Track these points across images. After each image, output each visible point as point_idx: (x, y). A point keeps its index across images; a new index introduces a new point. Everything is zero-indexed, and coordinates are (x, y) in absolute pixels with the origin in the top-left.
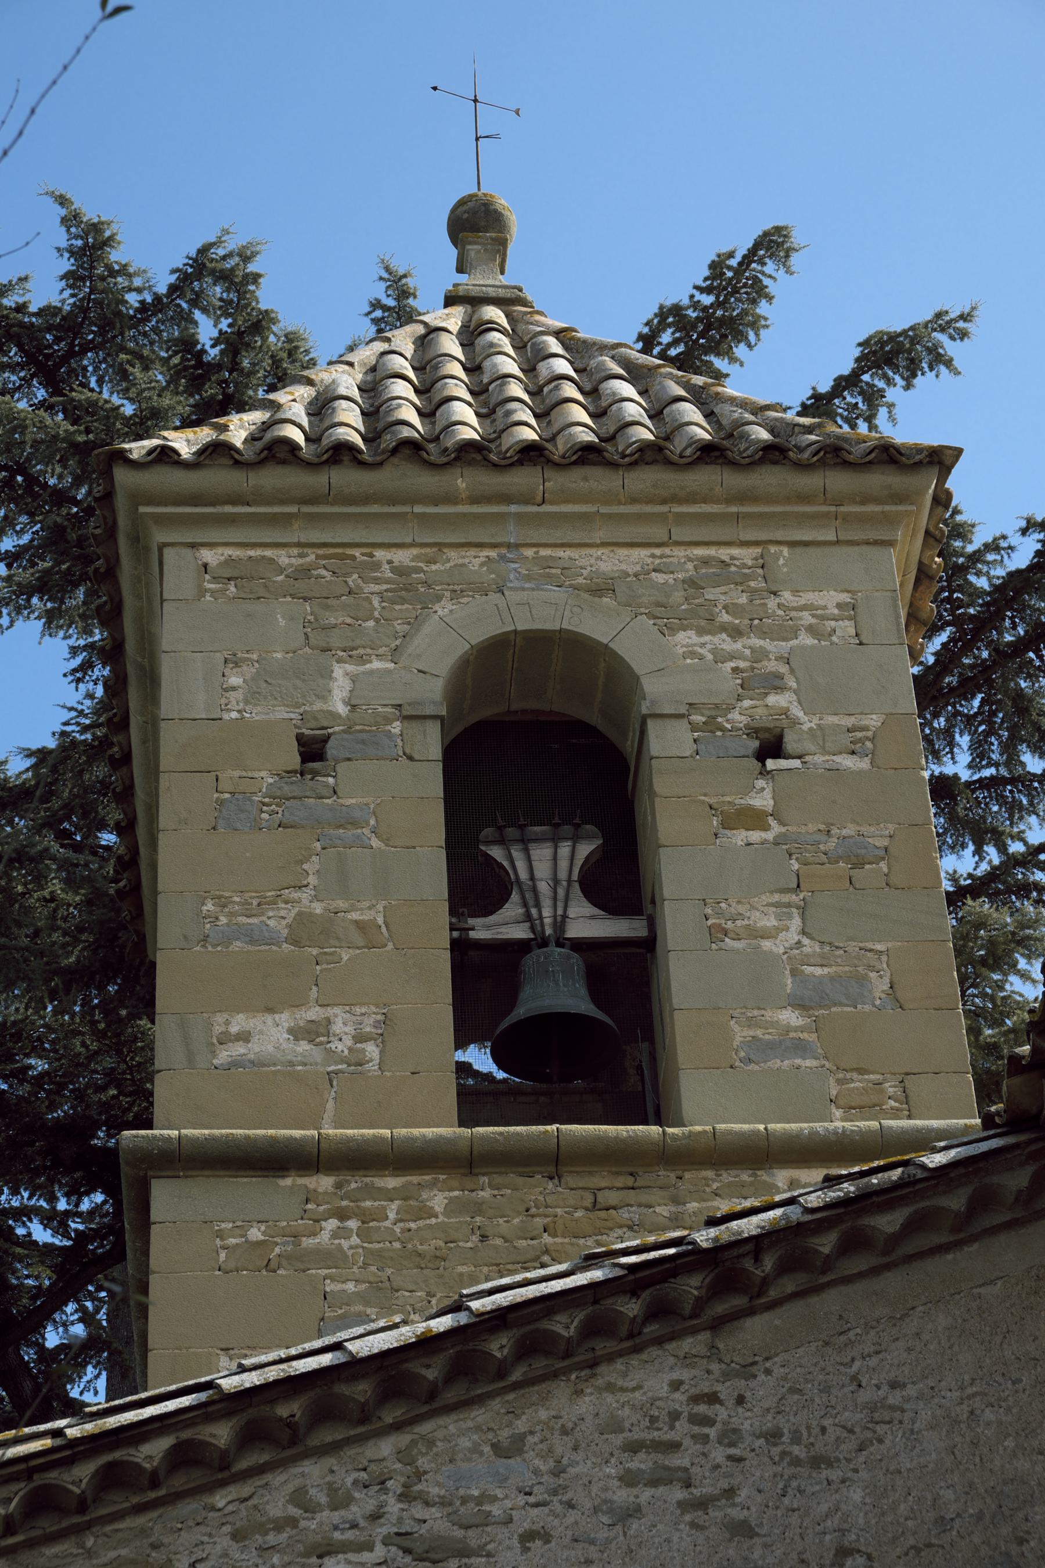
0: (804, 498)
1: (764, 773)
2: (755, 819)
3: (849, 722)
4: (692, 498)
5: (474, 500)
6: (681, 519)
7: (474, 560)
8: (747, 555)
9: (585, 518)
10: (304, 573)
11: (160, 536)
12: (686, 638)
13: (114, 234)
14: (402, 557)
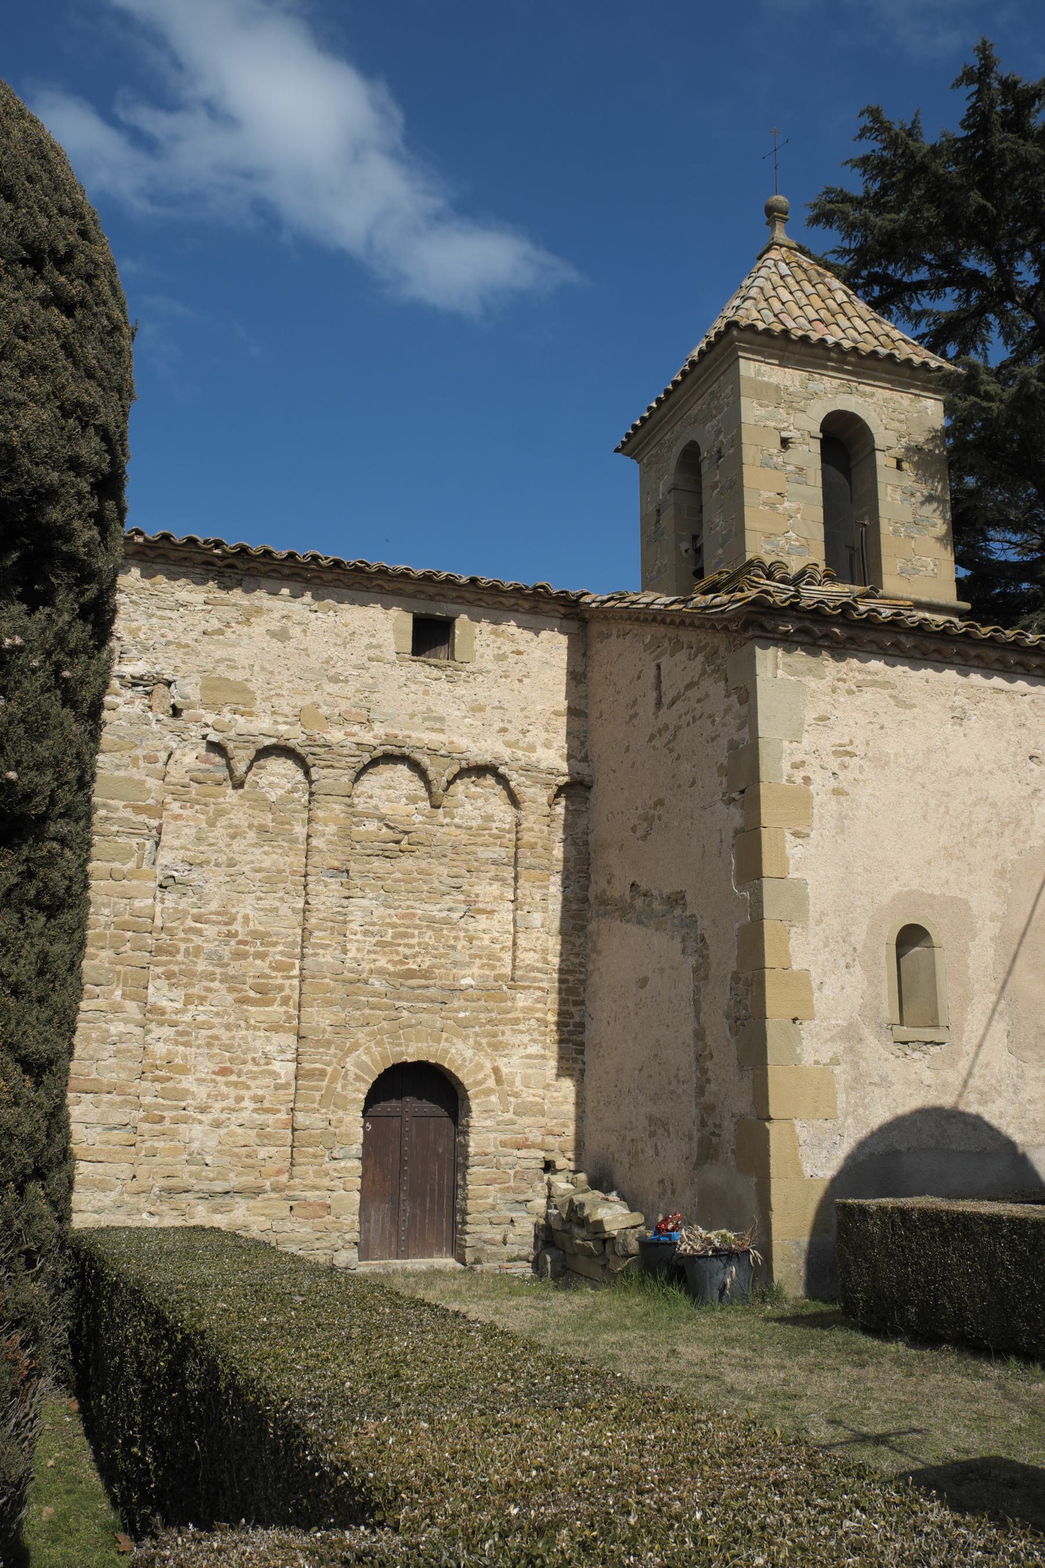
4: (699, 379)
7: (677, 428)
11: (740, 354)
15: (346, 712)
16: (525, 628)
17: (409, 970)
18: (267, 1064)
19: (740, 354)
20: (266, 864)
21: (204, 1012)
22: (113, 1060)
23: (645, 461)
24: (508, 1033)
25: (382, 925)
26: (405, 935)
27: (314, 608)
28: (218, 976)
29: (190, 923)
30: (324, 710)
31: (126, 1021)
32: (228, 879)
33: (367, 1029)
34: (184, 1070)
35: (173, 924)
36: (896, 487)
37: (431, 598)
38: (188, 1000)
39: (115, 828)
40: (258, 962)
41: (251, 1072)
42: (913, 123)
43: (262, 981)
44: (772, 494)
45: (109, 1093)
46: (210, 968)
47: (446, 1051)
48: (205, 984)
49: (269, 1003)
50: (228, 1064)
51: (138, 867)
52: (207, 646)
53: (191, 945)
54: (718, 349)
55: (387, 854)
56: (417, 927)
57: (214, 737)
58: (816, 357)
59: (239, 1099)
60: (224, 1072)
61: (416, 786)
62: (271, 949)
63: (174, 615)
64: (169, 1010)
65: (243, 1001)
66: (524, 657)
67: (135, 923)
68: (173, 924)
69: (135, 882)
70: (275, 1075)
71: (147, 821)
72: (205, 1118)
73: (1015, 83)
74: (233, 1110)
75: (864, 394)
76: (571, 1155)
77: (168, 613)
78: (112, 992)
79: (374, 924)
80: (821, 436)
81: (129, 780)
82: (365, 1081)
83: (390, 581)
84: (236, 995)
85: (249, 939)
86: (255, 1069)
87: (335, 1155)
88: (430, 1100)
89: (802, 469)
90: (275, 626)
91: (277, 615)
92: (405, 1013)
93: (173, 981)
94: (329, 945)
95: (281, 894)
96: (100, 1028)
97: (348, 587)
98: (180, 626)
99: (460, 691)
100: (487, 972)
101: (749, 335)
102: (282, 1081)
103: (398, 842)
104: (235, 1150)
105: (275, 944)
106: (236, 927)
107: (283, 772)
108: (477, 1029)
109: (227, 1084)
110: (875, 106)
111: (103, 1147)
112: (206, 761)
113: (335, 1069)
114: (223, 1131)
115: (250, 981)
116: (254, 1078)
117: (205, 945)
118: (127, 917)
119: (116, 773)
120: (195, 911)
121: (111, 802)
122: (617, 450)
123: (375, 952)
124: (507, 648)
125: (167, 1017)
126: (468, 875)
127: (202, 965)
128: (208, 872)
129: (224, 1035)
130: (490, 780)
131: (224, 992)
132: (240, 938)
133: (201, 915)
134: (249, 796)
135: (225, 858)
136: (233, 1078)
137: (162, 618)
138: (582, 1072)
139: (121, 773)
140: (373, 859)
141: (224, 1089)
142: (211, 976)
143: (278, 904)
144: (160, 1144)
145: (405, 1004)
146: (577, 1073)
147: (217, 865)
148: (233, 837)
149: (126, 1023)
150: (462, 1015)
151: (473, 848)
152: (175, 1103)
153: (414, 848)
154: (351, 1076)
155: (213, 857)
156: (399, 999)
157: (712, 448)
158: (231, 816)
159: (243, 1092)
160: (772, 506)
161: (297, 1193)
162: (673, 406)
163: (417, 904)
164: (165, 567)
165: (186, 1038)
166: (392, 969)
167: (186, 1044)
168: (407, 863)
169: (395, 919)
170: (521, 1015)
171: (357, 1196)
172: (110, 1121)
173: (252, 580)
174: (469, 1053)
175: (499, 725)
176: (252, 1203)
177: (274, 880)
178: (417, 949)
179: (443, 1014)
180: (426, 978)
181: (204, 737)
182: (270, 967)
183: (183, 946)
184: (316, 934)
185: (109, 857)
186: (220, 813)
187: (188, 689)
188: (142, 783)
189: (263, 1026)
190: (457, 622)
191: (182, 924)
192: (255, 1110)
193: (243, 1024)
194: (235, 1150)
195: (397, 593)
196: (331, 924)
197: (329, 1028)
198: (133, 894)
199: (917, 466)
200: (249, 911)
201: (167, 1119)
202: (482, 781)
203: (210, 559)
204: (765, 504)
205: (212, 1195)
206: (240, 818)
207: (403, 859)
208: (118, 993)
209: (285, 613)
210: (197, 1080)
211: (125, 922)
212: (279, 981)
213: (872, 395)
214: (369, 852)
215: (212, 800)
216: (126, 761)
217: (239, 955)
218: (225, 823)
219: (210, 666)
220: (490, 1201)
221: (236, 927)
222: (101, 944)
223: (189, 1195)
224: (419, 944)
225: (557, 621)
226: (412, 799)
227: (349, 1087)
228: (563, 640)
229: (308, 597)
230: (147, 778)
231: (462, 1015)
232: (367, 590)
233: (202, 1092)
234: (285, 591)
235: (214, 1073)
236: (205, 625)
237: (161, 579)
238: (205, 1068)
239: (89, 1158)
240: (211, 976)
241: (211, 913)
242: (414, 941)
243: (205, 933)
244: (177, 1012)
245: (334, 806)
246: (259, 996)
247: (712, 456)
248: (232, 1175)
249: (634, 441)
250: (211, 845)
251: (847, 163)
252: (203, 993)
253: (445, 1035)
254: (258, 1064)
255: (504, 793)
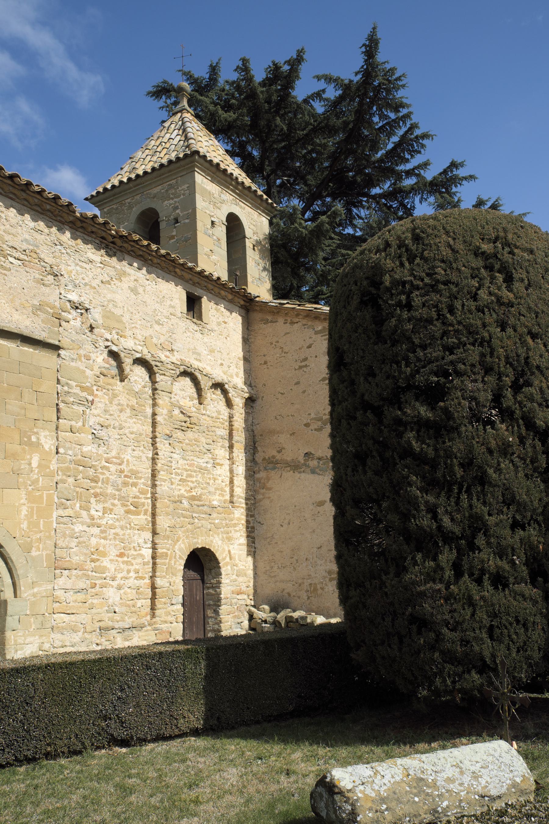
0: (179, 168)
1: (175, 227)
2: (173, 237)
3: (187, 212)
4: (163, 174)
5: (135, 187)
6: (164, 178)
7: (138, 197)
8: (174, 181)
9: (150, 184)
10: (117, 208)
11: (196, 169)
12: (166, 202)
13: (411, 113)
14: (129, 200)
15: (164, 343)
16: (227, 309)
17: (193, 495)
18: (140, 550)
19: (196, 169)
20: (135, 430)
21: (112, 519)
22: (77, 548)
23: (105, 210)
24: (233, 532)
25: (182, 469)
26: (191, 476)
27: (148, 277)
28: (117, 497)
29: (104, 463)
30: (155, 340)
31: (83, 523)
32: (119, 437)
33: (183, 529)
34: (104, 555)
35: (96, 463)
36: (253, 259)
37: (194, 284)
38: (105, 511)
39: (72, 399)
40: (134, 488)
41: (133, 555)
42: (217, 63)
43: (136, 500)
44: (208, 250)
45: (76, 569)
46: (114, 492)
47: (212, 541)
48: (112, 501)
49: (138, 514)
50: (123, 551)
51: (84, 426)
52: (104, 290)
53: (105, 477)
54: (182, 163)
55: (183, 428)
56: (195, 471)
57: (115, 348)
58: (226, 182)
59: (129, 571)
60: (121, 555)
61: (191, 390)
62: (139, 481)
63: (88, 266)
64: (96, 517)
65: (128, 512)
66: (227, 325)
67: (84, 461)
68: (96, 463)
69: (82, 435)
70: (142, 556)
71: (87, 396)
72: (115, 583)
73: (276, 67)
74: (126, 578)
75: (241, 207)
76: (251, 597)
77: (84, 265)
78: (75, 504)
79: (179, 469)
80: (226, 224)
81: (78, 369)
82: (183, 559)
83: (183, 270)
84: (125, 508)
85: (129, 474)
86: (135, 553)
87: (173, 602)
88: (193, 571)
89: (219, 240)
90: (132, 284)
91: (132, 278)
92: (196, 520)
93: (98, 499)
94: (166, 480)
95: (142, 448)
96: (70, 528)
97: (162, 269)
98: (91, 275)
99: (206, 340)
100: (221, 498)
101: (202, 161)
102: (146, 560)
103: (185, 422)
104: (128, 602)
105: (141, 478)
106: (123, 467)
107: (141, 374)
108: (222, 530)
109: (123, 562)
110: (247, 58)
111: (74, 604)
112: (107, 363)
113: (171, 553)
114: (122, 591)
115: (131, 500)
116: (135, 559)
117: (111, 477)
118: (80, 457)
119: (72, 364)
120: (106, 455)
121: (70, 382)
122: (86, 199)
123: (180, 485)
124: (221, 319)
125: (95, 521)
126: (212, 443)
127: (110, 490)
128: (111, 431)
129: (121, 532)
130: (219, 392)
131: (120, 506)
132: (125, 473)
133: (109, 459)
134: (127, 387)
135: (118, 424)
136: (125, 559)
137: (82, 267)
138: (255, 552)
139: (73, 364)
140: (177, 430)
141: (122, 566)
142: (113, 497)
143: (141, 454)
144: (95, 601)
145: (197, 515)
146: (252, 553)
147: (114, 428)
148: (121, 412)
149: (82, 525)
150: (217, 521)
151: (213, 429)
152: (101, 575)
153: (193, 426)
154: (178, 556)
155: (112, 423)
156: (193, 512)
157: (170, 216)
158: (119, 398)
159: (130, 567)
160: (208, 256)
161: (158, 626)
162: (138, 185)
163: (195, 458)
164: (82, 235)
165: (104, 535)
166: (186, 495)
167: (105, 538)
168: (190, 434)
169: (187, 467)
170: (237, 522)
171: (181, 626)
172: (77, 587)
173: (120, 253)
174: (220, 543)
175: (220, 362)
176: (141, 633)
177: (139, 439)
178: (195, 484)
179: (210, 521)
180: (200, 501)
181: (107, 347)
182: (139, 492)
183: (101, 477)
184: (162, 473)
185: (70, 418)
186: (115, 396)
187: (96, 315)
188: (84, 372)
189: (137, 527)
190: (203, 299)
191: (100, 463)
192: (136, 578)
193: (128, 526)
194: (128, 602)
195: (181, 278)
196: (166, 467)
197: (168, 528)
198: (83, 442)
199: (260, 251)
200: (128, 457)
201: (98, 585)
202: (216, 391)
203: (105, 236)
204: (206, 254)
205: (124, 630)
206: (123, 399)
207: (189, 432)
208: (78, 505)
209: (136, 278)
210: (110, 560)
211: (79, 460)
212: (143, 500)
213: (244, 209)
214: (176, 427)
215: (110, 387)
216: (75, 357)
217: (125, 484)
218: (117, 402)
219: (106, 303)
220: (229, 623)
221: (123, 467)
222: (68, 474)
223: (114, 631)
224: (196, 481)
225: (238, 308)
226: (192, 399)
227: (177, 563)
228: (240, 318)
229: (144, 271)
230: (86, 369)
231: (217, 521)
232: (169, 272)
233: (112, 567)
234: (135, 264)
235: (117, 556)
236: (101, 278)
237: (79, 241)
238: (113, 553)
239: (68, 612)
240: (113, 497)
241: (113, 458)
242: (194, 479)
243: (111, 469)
244: (100, 518)
245: (166, 398)
246: (135, 509)
247: (169, 220)
248: (126, 618)
249: (101, 197)
250: (111, 415)
251: (180, 71)
252: (111, 507)
253: (211, 532)
254: (136, 551)
255: (224, 400)
